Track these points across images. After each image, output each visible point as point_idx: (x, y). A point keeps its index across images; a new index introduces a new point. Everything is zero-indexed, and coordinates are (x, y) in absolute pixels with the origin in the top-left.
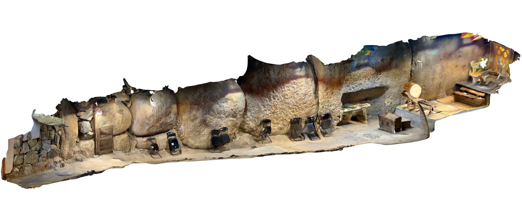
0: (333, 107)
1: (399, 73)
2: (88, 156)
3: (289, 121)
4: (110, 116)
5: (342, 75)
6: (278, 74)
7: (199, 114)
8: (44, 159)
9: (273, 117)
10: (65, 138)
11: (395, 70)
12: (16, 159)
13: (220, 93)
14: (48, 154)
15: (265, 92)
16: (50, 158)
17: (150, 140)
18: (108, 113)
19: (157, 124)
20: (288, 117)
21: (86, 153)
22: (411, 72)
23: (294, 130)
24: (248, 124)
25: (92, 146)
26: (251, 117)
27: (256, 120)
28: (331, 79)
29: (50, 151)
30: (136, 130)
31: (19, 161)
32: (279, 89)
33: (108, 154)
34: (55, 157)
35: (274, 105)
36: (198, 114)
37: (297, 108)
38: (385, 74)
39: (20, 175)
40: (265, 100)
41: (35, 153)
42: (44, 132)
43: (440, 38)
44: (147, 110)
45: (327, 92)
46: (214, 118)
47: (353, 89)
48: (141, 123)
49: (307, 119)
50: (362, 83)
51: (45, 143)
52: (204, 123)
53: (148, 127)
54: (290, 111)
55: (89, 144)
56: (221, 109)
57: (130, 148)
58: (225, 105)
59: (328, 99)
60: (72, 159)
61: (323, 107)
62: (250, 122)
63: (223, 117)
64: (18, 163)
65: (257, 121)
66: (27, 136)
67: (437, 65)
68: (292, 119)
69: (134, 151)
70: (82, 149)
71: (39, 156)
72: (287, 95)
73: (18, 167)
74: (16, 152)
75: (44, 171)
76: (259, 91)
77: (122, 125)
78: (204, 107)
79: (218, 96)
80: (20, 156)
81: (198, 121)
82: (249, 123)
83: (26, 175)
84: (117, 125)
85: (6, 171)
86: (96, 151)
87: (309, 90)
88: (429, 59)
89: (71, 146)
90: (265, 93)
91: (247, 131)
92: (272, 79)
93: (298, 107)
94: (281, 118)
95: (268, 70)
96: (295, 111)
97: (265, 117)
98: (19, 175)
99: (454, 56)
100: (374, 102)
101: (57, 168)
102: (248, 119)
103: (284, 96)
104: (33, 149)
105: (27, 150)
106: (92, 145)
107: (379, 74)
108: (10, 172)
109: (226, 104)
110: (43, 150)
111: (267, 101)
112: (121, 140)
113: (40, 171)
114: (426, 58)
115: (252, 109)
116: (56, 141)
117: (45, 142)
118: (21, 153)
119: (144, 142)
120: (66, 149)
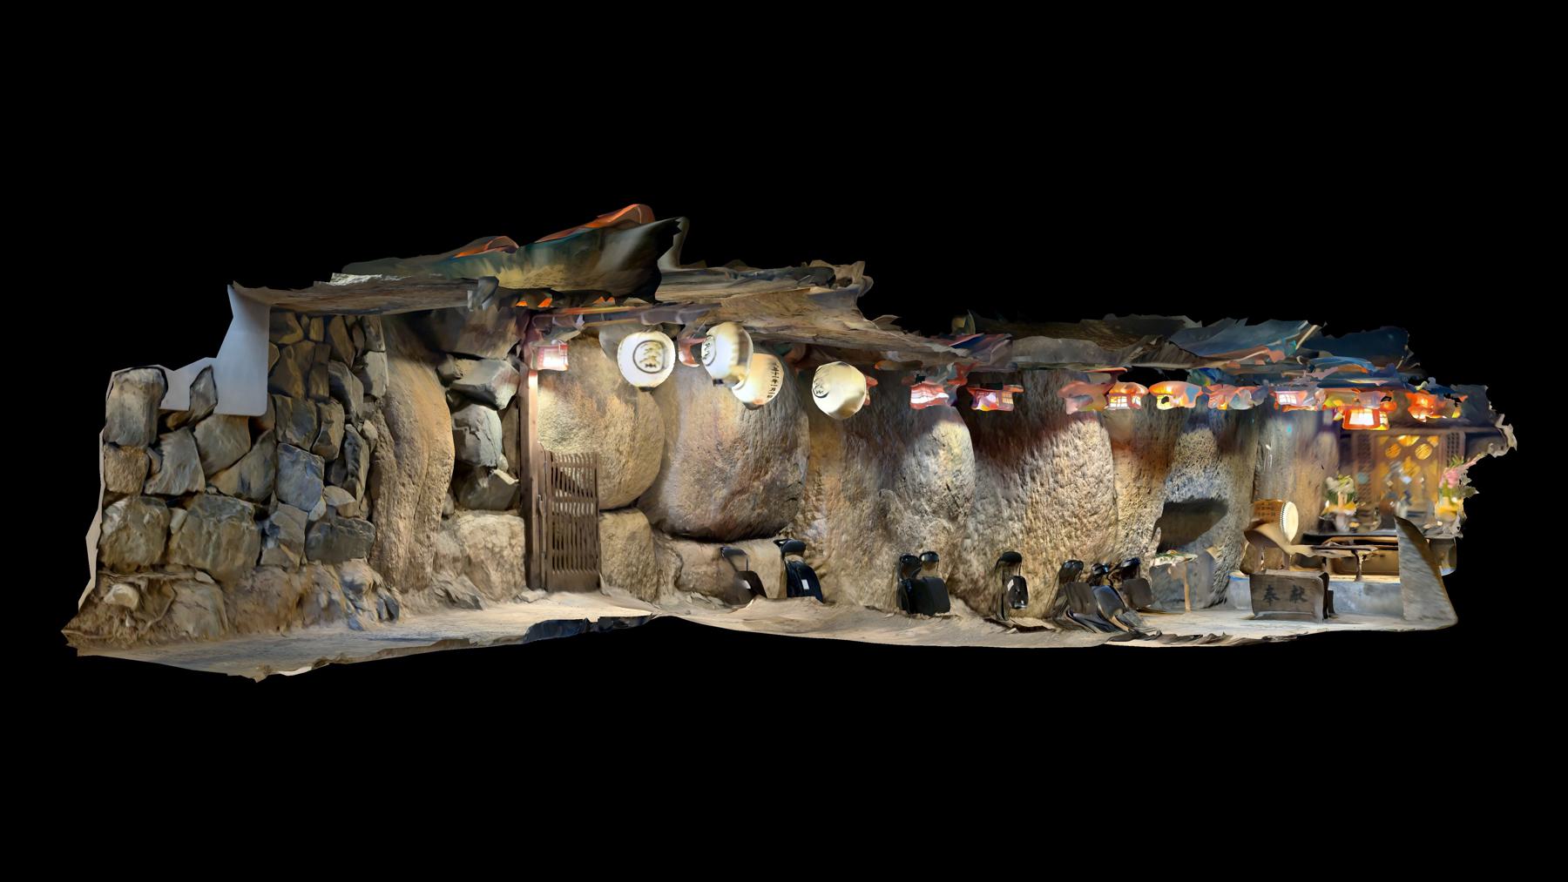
2: (498, 591)
4: (587, 403)
6: (1046, 391)
8: (291, 555)
9: (1026, 546)
10: (399, 464)
12: (116, 517)
14: (314, 534)
16: (324, 562)
17: (728, 556)
18: (578, 384)
19: (755, 484)
20: (1057, 554)
21: (488, 575)
23: (1077, 599)
25: (513, 542)
27: (987, 549)
28: (1150, 441)
29: (324, 518)
30: (676, 503)
31: (142, 541)
32: (1047, 447)
34: (348, 559)
35: (1032, 504)
39: (143, 630)
40: (1011, 479)
41: (239, 508)
42: (289, 399)
44: (723, 412)
45: (1138, 485)
48: (698, 472)
49: (1094, 568)
51: (294, 463)
52: (882, 521)
53: (724, 492)
55: (499, 528)
58: (929, 461)
60: (426, 591)
62: (973, 554)
63: (926, 511)
64: (131, 550)
66: (192, 386)
68: (1065, 563)
70: (469, 547)
71: (264, 536)
73: (131, 579)
74: (116, 472)
75: (293, 629)
76: (997, 442)
77: (631, 464)
80: (143, 508)
82: (969, 558)
83: (187, 639)
84: (614, 456)
86: (534, 569)
89: (422, 517)
90: (1013, 455)
91: (962, 588)
92: (1030, 406)
98: (135, 629)
101: (363, 619)
104: (228, 481)
105: (193, 481)
106: (513, 536)
109: (933, 461)
110: (283, 502)
112: (627, 534)
113: (267, 625)
116: (350, 467)
117: (293, 458)
118: (149, 491)
119: (708, 564)
120: (402, 529)
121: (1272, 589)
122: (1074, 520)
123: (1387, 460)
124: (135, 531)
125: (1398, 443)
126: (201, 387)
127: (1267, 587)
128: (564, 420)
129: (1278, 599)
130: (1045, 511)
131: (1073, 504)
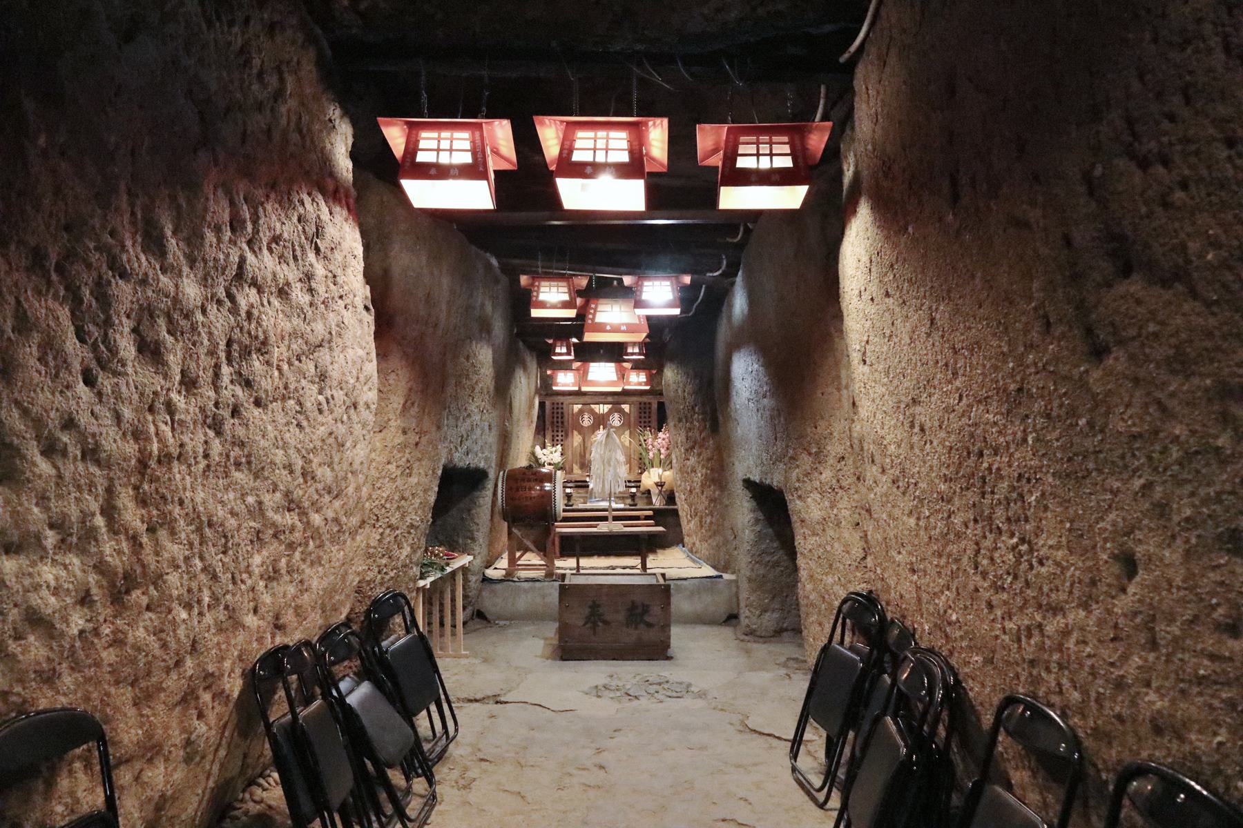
9: (109, 656)
121: (599, 606)
122: (290, 519)
127: (590, 603)
129: (606, 623)
130: (200, 495)
131: (289, 467)
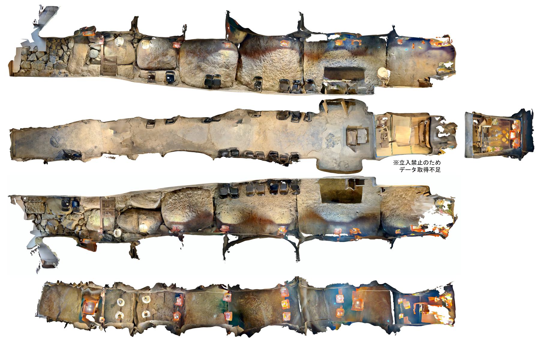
0: (314, 76)
1: (375, 60)
3: (279, 81)
5: (319, 51)
6: (267, 43)
7: (195, 60)
11: (370, 57)
13: (214, 48)
15: (257, 55)
19: (155, 61)
22: (386, 61)
24: (244, 78)
26: (246, 73)
29: (56, 64)
33: (111, 76)
36: (193, 60)
37: (284, 71)
38: (361, 58)
43: (413, 40)
46: (209, 66)
47: (333, 65)
50: (341, 61)
53: (147, 62)
54: (278, 73)
56: (215, 61)
57: (134, 76)
58: (219, 58)
59: (310, 68)
61: (307, 74)
65: (251, 77)
67: (409, 60)
69: (137, 79)
72: (274, 60)
78: (199, 56)
79: (213, 50)
81: (193, 65)
82: (244, 77)
85: (13, 70)
87: (293, 59)
88: (401, 54)
93: (285, 71)
94: (271, 77)
95: (259, 39)
96: (282, 73)
97: (257, 75)
99: (424, 55)
100: (362, 83)
102: (243, 74)
103: (272, 60)
107: (355, 57)
108: (17, 72)
111: (258, 62)
114: (399, 52)
115: (246, 67)
123: (502, 130)
124: (25, 64)
125: (507, 133)
126: (35, 48)
128: (110, 51)
